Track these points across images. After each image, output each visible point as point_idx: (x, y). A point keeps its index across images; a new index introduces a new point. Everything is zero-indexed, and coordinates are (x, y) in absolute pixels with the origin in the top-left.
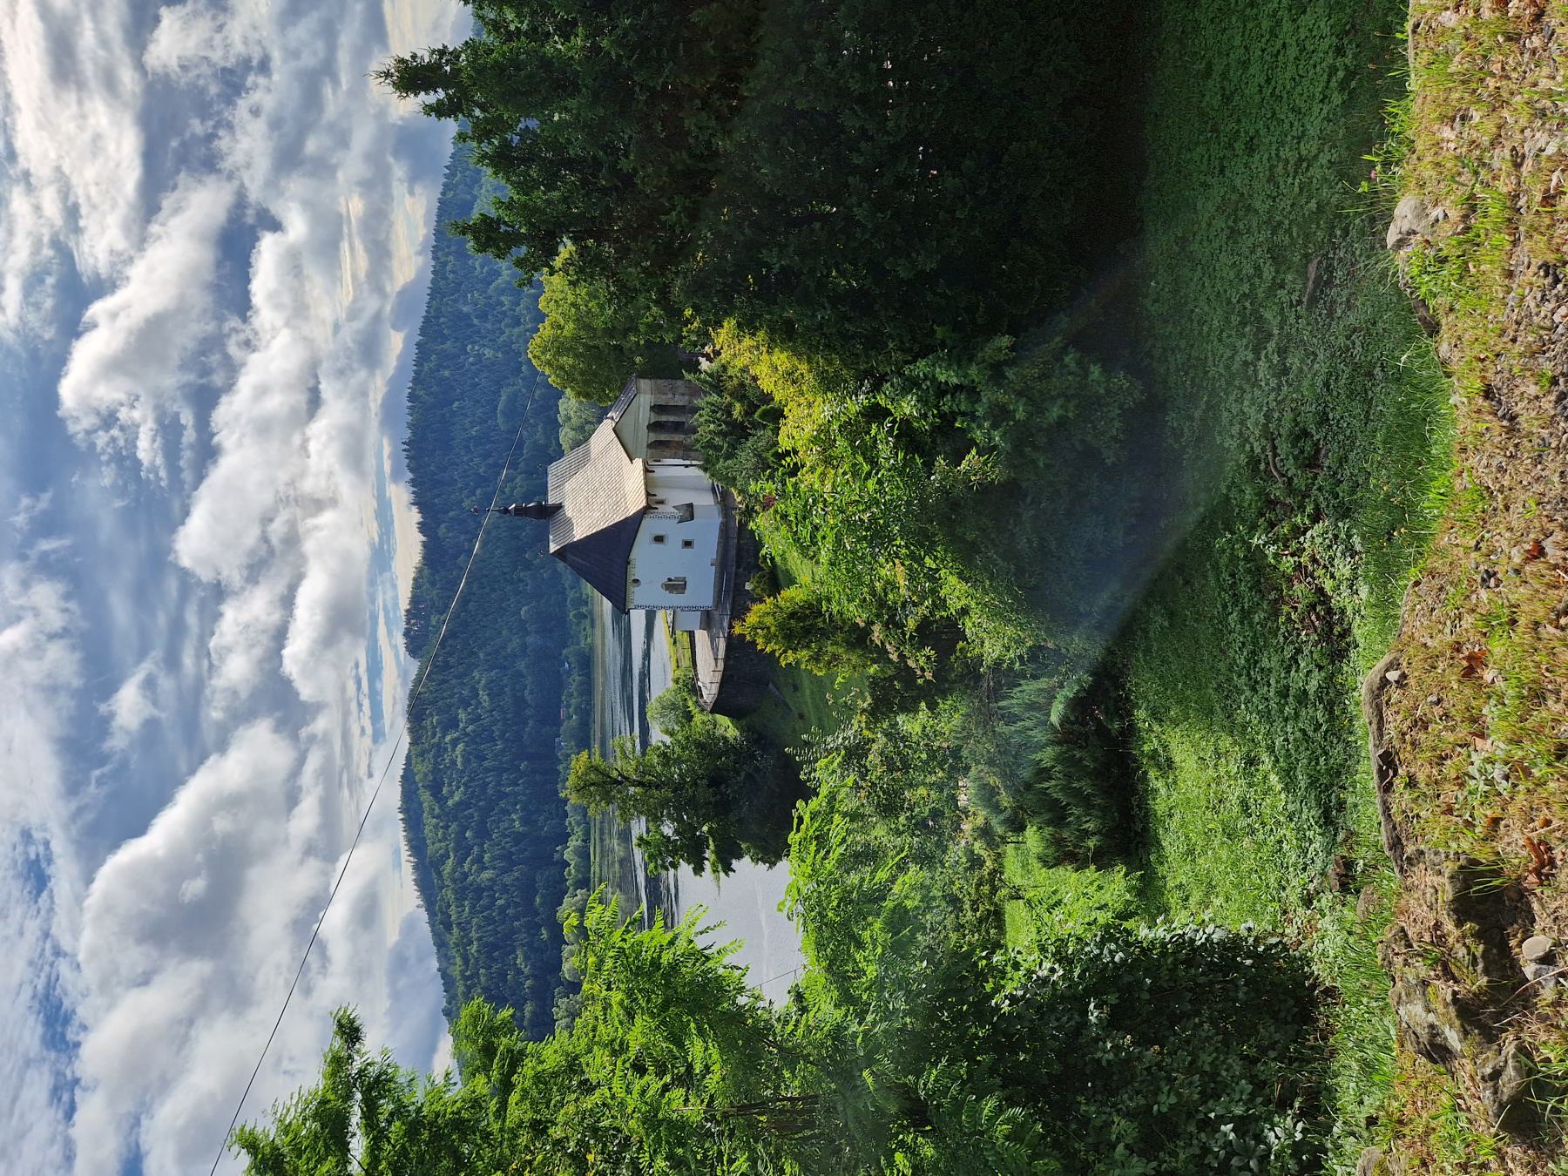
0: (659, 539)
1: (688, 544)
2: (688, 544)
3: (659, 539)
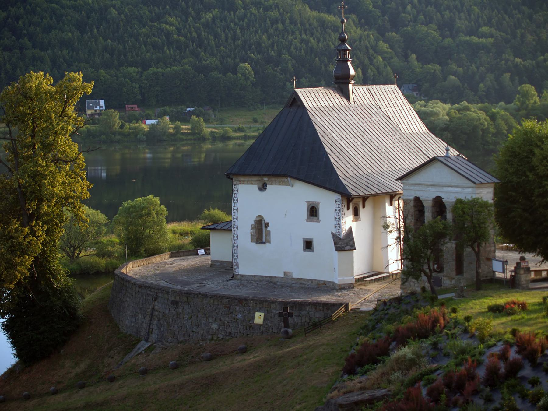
0: (313, 212)
1: (308, 245)
2: (308, 245)
3: (313, 212)
